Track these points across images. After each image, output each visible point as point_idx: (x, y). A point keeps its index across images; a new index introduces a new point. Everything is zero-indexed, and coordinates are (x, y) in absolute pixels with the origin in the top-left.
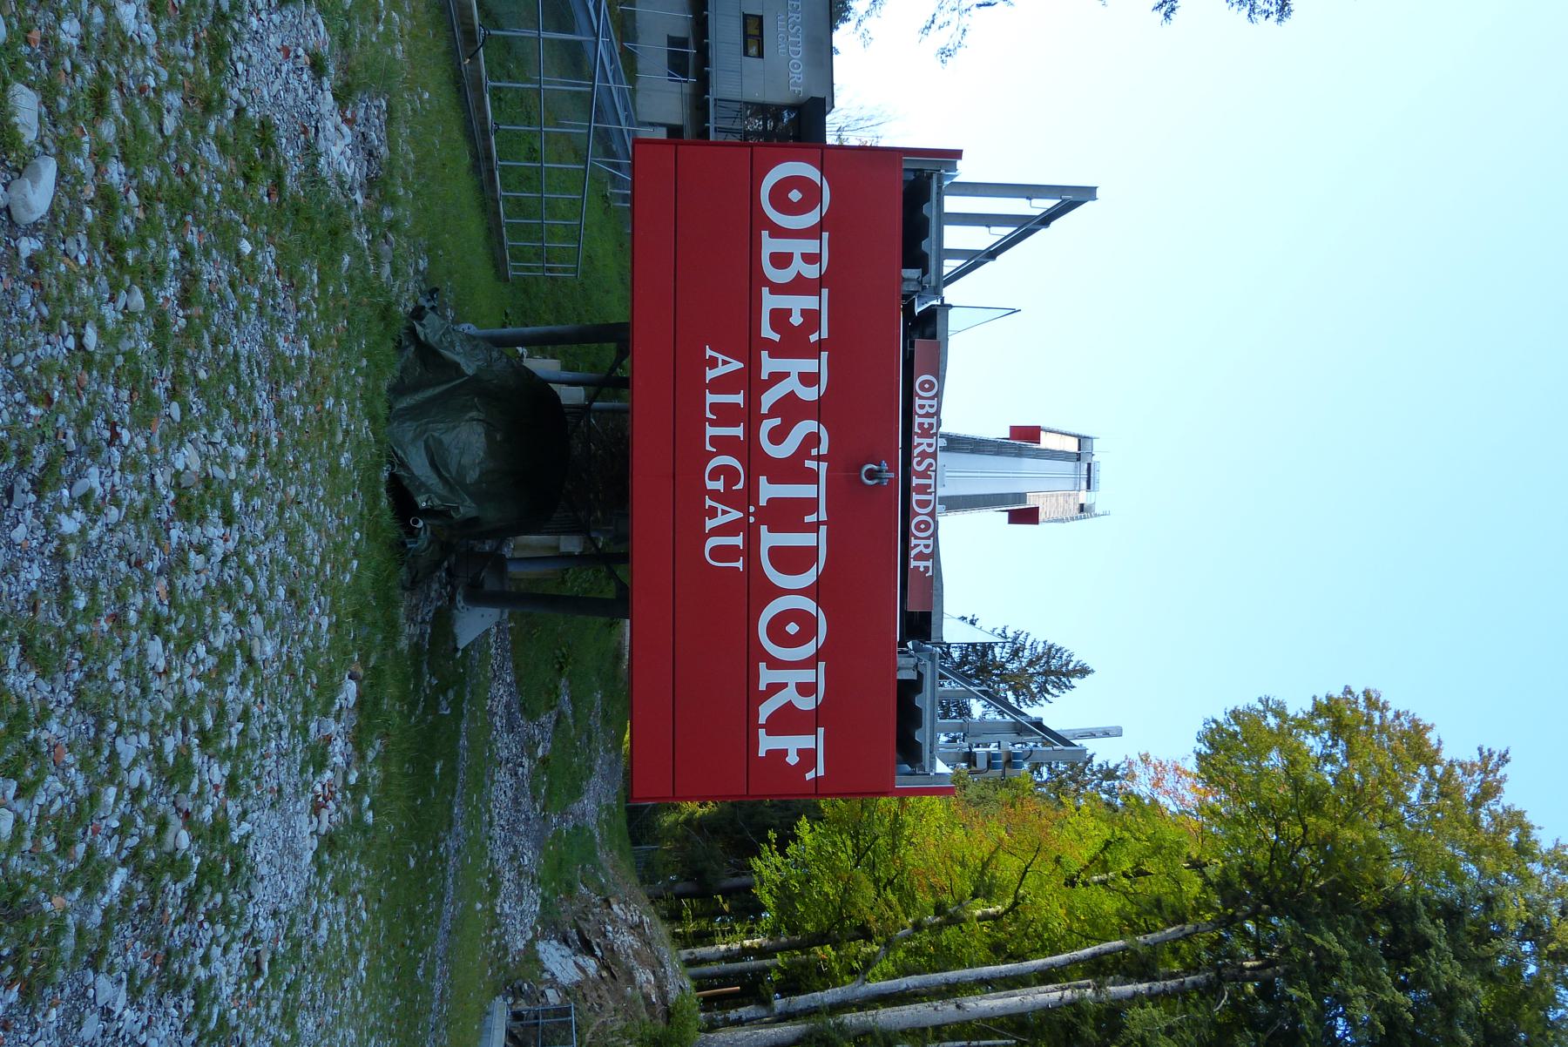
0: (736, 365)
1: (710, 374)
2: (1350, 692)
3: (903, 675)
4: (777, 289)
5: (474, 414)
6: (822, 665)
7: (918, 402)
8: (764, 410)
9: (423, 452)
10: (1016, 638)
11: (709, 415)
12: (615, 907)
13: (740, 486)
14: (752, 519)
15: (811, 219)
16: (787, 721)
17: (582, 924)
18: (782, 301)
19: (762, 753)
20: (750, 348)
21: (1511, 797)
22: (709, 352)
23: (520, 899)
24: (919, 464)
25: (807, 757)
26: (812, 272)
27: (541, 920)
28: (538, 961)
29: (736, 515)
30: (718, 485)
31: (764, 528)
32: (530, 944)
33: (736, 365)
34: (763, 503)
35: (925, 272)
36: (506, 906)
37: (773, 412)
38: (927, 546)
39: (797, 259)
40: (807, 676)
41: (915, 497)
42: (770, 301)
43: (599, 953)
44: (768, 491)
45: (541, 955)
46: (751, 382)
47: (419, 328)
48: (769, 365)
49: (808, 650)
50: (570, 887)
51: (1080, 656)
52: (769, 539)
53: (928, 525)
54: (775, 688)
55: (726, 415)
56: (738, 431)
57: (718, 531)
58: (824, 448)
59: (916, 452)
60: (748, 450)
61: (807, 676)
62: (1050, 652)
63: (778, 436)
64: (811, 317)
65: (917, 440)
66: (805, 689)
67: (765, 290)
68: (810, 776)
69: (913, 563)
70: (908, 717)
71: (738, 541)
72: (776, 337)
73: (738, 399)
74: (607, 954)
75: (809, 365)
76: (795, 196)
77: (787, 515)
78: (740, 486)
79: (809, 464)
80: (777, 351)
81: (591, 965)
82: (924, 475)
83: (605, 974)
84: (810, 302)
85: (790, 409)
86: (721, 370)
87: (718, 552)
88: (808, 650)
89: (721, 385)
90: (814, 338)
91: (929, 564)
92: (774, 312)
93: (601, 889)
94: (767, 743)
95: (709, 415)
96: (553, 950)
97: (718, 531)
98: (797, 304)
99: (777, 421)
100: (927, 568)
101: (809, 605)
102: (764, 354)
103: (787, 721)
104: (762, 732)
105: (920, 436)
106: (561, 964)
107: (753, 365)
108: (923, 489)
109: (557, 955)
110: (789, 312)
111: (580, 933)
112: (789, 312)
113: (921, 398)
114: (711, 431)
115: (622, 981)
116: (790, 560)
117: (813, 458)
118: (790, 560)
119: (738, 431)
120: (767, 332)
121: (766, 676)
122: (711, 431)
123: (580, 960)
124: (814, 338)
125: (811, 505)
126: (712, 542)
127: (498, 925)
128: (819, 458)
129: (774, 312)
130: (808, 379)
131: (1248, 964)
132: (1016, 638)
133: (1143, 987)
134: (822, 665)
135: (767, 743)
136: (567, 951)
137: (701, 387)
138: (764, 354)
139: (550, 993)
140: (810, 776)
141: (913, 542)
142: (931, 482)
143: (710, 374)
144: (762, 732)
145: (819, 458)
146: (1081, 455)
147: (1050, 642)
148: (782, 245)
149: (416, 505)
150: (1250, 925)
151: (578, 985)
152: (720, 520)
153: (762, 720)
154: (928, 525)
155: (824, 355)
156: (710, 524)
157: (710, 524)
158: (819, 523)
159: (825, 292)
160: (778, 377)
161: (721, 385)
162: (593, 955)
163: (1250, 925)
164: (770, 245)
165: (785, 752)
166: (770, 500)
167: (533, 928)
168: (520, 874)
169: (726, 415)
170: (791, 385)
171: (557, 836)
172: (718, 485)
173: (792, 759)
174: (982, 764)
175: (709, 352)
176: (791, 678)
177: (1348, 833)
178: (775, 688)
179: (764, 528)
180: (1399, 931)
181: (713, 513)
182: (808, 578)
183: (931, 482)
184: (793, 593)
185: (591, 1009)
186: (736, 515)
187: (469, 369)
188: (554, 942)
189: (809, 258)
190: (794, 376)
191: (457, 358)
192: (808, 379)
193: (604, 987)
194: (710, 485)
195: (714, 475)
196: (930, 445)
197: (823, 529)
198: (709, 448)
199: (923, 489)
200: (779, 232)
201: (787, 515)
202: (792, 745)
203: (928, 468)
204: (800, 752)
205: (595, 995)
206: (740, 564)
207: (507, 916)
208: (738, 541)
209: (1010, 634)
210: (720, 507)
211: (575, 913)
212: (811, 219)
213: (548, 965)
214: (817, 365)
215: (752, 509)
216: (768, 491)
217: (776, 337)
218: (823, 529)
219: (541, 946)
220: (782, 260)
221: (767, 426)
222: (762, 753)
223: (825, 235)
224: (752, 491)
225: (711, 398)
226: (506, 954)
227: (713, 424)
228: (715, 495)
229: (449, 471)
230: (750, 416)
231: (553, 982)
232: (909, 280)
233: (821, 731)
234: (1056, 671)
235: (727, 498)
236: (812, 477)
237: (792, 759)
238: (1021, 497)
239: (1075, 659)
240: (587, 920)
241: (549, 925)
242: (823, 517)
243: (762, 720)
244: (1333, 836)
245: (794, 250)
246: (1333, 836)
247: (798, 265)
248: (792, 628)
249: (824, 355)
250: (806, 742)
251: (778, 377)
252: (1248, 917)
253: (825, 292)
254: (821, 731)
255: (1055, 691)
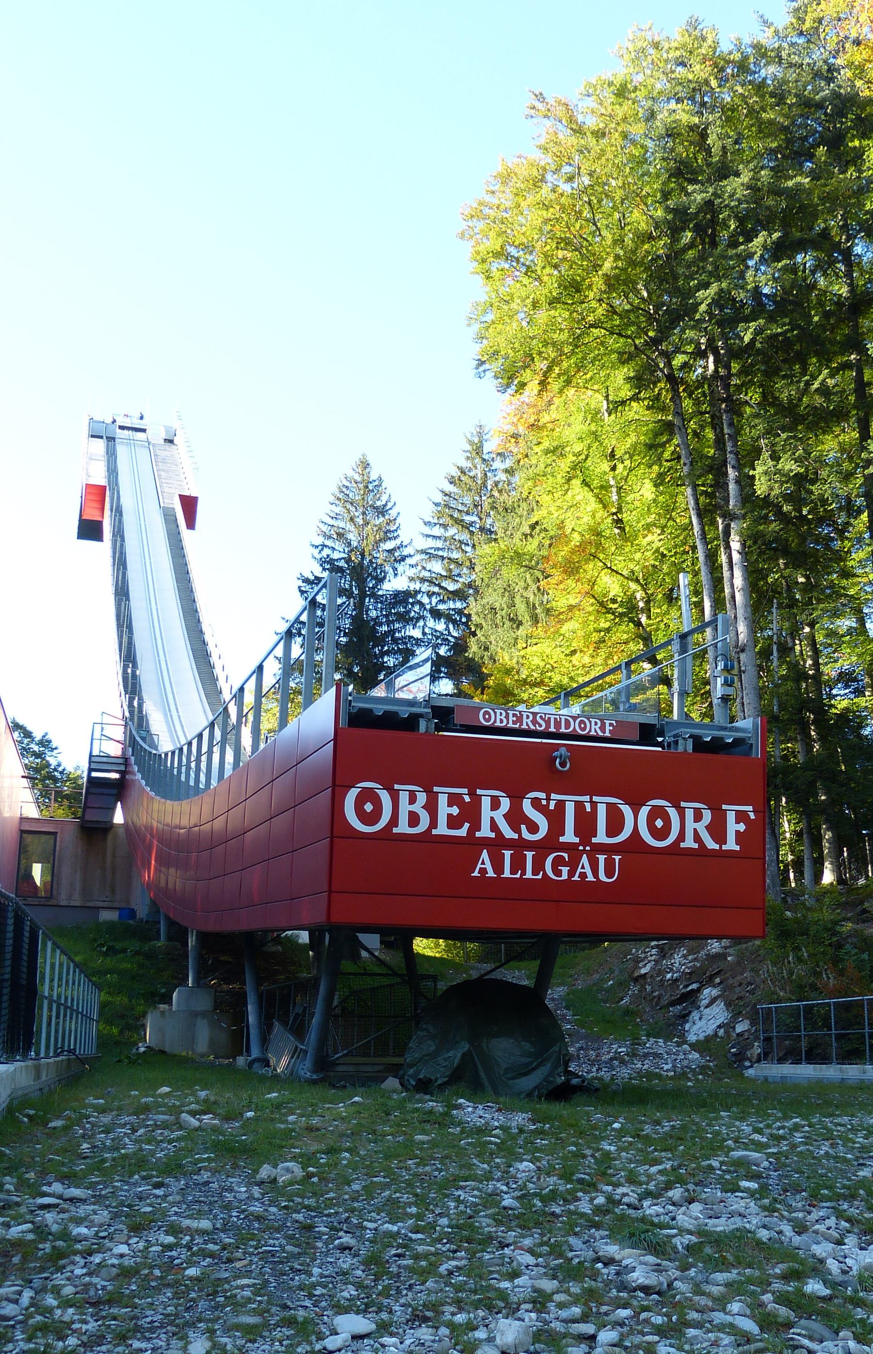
0: (485, 854)
1: (491, 873)
2: (463, 234)
3: (690, 749)
4: (434, 824)
5: (484, 1046)
6: (683, 804)
7: (498, 724)
8: (516, 836)
9: (517, 1081)
10: (325, 535)
11: (518, 876)
12: (643, 971)
13: (566, 855)
14: (588, 848)
15: (385, 797)
16: (718, 830)
17: (664, 1001)
18: (442, 820)
19: (738, 848)
20: (473, 844)
21: (572, 93)
22: (476, 874)
23: (657, 1055)
24: (540, 726)
25: (741, 817)
26: (422, 798)
27: (668, 1038)
28: (708, 1039)
29: (585, 859)
30: (565, 870)
31: (594, 840)
32: (694, 1046)
33: (485, 854)
34: (577, 840)
35: (421, 715)
36: (666, 1067)
37: (518, 831)
38: (596, 724)
39: (412, 808)
40: (689, 815)
41: (563, 730)
42: (442, 829)
43: (694, 986)
44: (569, 836)
45: (702, 1037)
46: (497, 844)
47: (439, 1082)
48: (485, 832)
49: (673, 812)
50: (627, 1012)
51: (347, 468)
52: (601, 837)
53: (582, 722)
54: (697, 838)
55: (518, 864)
56: (529, 855)
57: (595, 873)
58: (542, 795)
59: (532, 727)
60: (543, 848)
61: (689, 815)
62: (344, 498)
63: (533, 828)
64: (453, 800)
65: (524, 726)
66: (698, 817)
67: (434, 832)
68: (752, 816)
69: (607, 734)
70: (717, 746)
71: (602, 858)
72: (467, 825)
73: (508, 854)
74: (694, 978)
75: (486, 803)
76: (368, 807)
77: (586, 824)
78: (566, 855)
79: (552, 806)
80: (476, 825)
81: (708, 992)
82: (548, 723)
83: (718, 980)
84: (443, 800)
85: (516, 818)
86: (488, 866)
87: (609, 873)
88: (673, 812)
89: (498, 866)
90: (467, 799)
91: (607, 722)
92: (450, 827)
93: (622, 985)
94: (731, 845)
95: (518, 876)
96: (695, 1027)
97: (595, 873)
98: (444, 810)
99: (523, 827)
100: (611, 724)
101: (644, 811)
102: (478, 834)
103: (718, 830)
104: (724, 847)
105: (521, 724)
106: (708, 1019)
107: (485, 843)
108: (558, 724)
109: (699, 1024)
110: (450, 816)
111: (673, 1004)
112: (450, 816)
113: (495, 721)
114: (529, 875)
115: (722, 965)
116: (615, 824)
117: (548, 804)
118: (615, 824)
119: (529, 855)
120: (463, 832)
121: (689, 843)
122: (529, 875)
123: (705, 1002)
124: (467, 799)
125: (579, 806)
126: (602, 877)
127: (684, 1074)
128: (548, 799)
129: (450, 827)
130: (495, 804)
131: (711, 367)
132: (325, 535)
133: (732, 473)
134: (683, 804)
135: (731, 845)
136: (695, 1015)
137: (499, 880)
138: (478, 834)
139: (739, 1028)
140: (752, 816)
141: (593, 733)
142: (552, 717)
143: (491, 873)
144: (724, 847)
145: (548, 799)
146: (106, 435)
147: (332, 499)
148: (403, 819)
149: (563, 1084)
150: (679, 360)
151: (728, 1005)
152: (588, 870)
153: (717, 847)
154: (582, 722)
155: (479, 792)
156: (590, 878)
157: (590, 878)
158: (591, 802)
159: (436, 789)
160: (494, 826)
161: (498, 866)
162: (699, 990)
163: (679, 360)
164: (403, 827)
165: (737, 832)
166: (576, 835)
167: (679, 1045)
168: (635, 1055)
169: (518, 864)
170: (499, 816)
171: (581, 1024)
172: (565, 870)
173: (742, 827)
174: (730, 691)
175: (476, 874)
176: (690, 825)
177: (608, 265)
178: (697, 838)
179: (594, 840)
180: (695, 233)
181: (583, 875)
182: (627, 810)
183: (552, 717)
184: (636, 821)
185: (752, 992)
186: (585, 859)
187: (467, 1047)
188: (687, 1027)
189: (412, 800)
190: (493, 814)
191: (459, 1055)
192: (495, 804)
193: (731, 981)
194: (565, 876)
195: (558, 873)
196: (528, 717)
197: (595, 799)
198: (540, 877)
199: (558, 724)
200: (394, 821)
201: (586, 824)
202: (733, 827)
203: (544, 720)
204: (737, 822)
205: (738, 990)
206: (617, 858)
207: (674, 1066)
208: (602, 858)
209: (319, 540)
210: (579, 870)
211: (653, 1007)
212: (385, 797)
213: (710, 1031)
214: (486, 796)
215: (581, 848)
216: (569, 836)
217: (467, 825)
218: (595, 799)
219: (692, 1038)
220: (414, 819)
221: (526, 835)
222: (738, 848)
223: (396, 787)
224: (569, 847)
225: (507, 874)
226: (708, 1067)
227: (524, 873)
228: (571, 873)
229: (532, 1062)
230: (520, 846)
231: (728, 1026)
232: (427, 728)
233: (724, 807)
234: (365, 498)
235: (573, 865)
236: (561, 804)
237: (742, 827)
238: (169, 517)
239: (351, 473)
240: (659, 997)
241: (673, 1029)
242: (587, 798)
243: (717, 847)
244: (607, 278)
245: (408, 810)
246: (607, 278)
247: (417, 807)
248: (659, 823)
249: (479, 792)
250: (731, 817)
251: (494, 826)
252: (669, 364)
253: (436, 789)
254: (724, 807)
255: (384, 498)
